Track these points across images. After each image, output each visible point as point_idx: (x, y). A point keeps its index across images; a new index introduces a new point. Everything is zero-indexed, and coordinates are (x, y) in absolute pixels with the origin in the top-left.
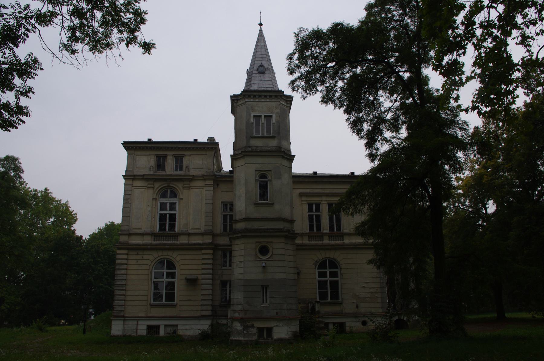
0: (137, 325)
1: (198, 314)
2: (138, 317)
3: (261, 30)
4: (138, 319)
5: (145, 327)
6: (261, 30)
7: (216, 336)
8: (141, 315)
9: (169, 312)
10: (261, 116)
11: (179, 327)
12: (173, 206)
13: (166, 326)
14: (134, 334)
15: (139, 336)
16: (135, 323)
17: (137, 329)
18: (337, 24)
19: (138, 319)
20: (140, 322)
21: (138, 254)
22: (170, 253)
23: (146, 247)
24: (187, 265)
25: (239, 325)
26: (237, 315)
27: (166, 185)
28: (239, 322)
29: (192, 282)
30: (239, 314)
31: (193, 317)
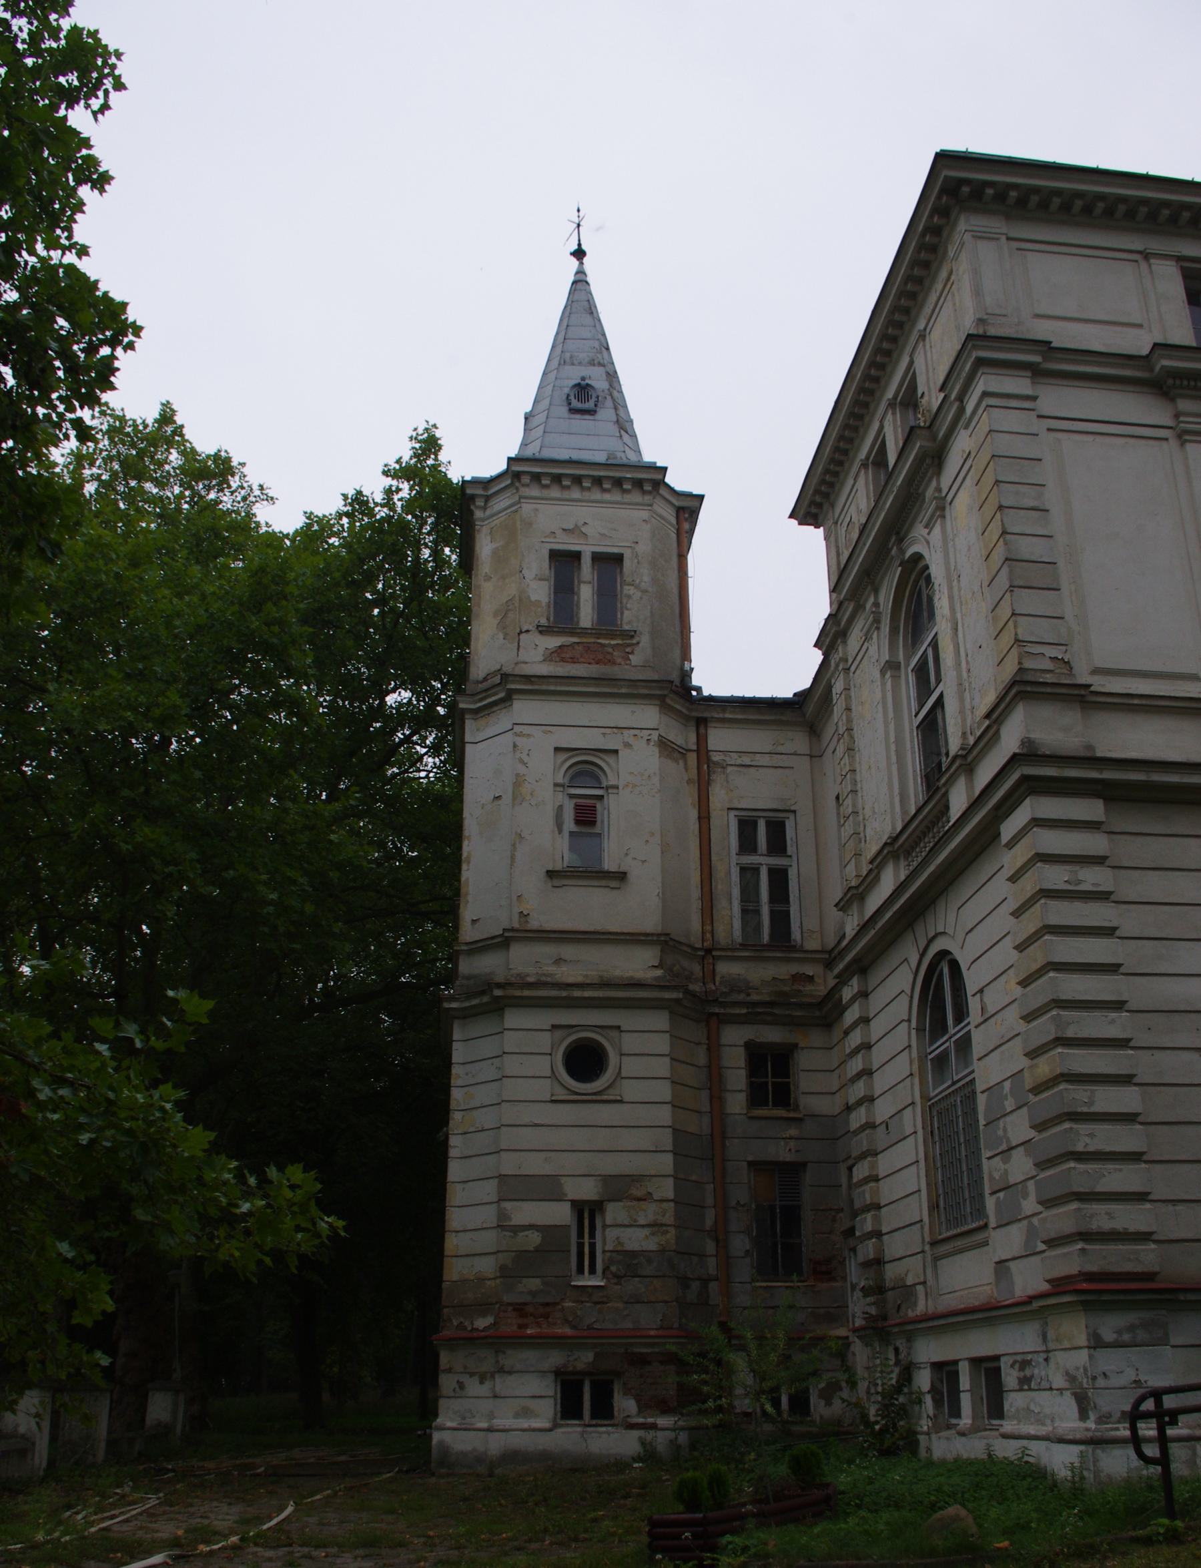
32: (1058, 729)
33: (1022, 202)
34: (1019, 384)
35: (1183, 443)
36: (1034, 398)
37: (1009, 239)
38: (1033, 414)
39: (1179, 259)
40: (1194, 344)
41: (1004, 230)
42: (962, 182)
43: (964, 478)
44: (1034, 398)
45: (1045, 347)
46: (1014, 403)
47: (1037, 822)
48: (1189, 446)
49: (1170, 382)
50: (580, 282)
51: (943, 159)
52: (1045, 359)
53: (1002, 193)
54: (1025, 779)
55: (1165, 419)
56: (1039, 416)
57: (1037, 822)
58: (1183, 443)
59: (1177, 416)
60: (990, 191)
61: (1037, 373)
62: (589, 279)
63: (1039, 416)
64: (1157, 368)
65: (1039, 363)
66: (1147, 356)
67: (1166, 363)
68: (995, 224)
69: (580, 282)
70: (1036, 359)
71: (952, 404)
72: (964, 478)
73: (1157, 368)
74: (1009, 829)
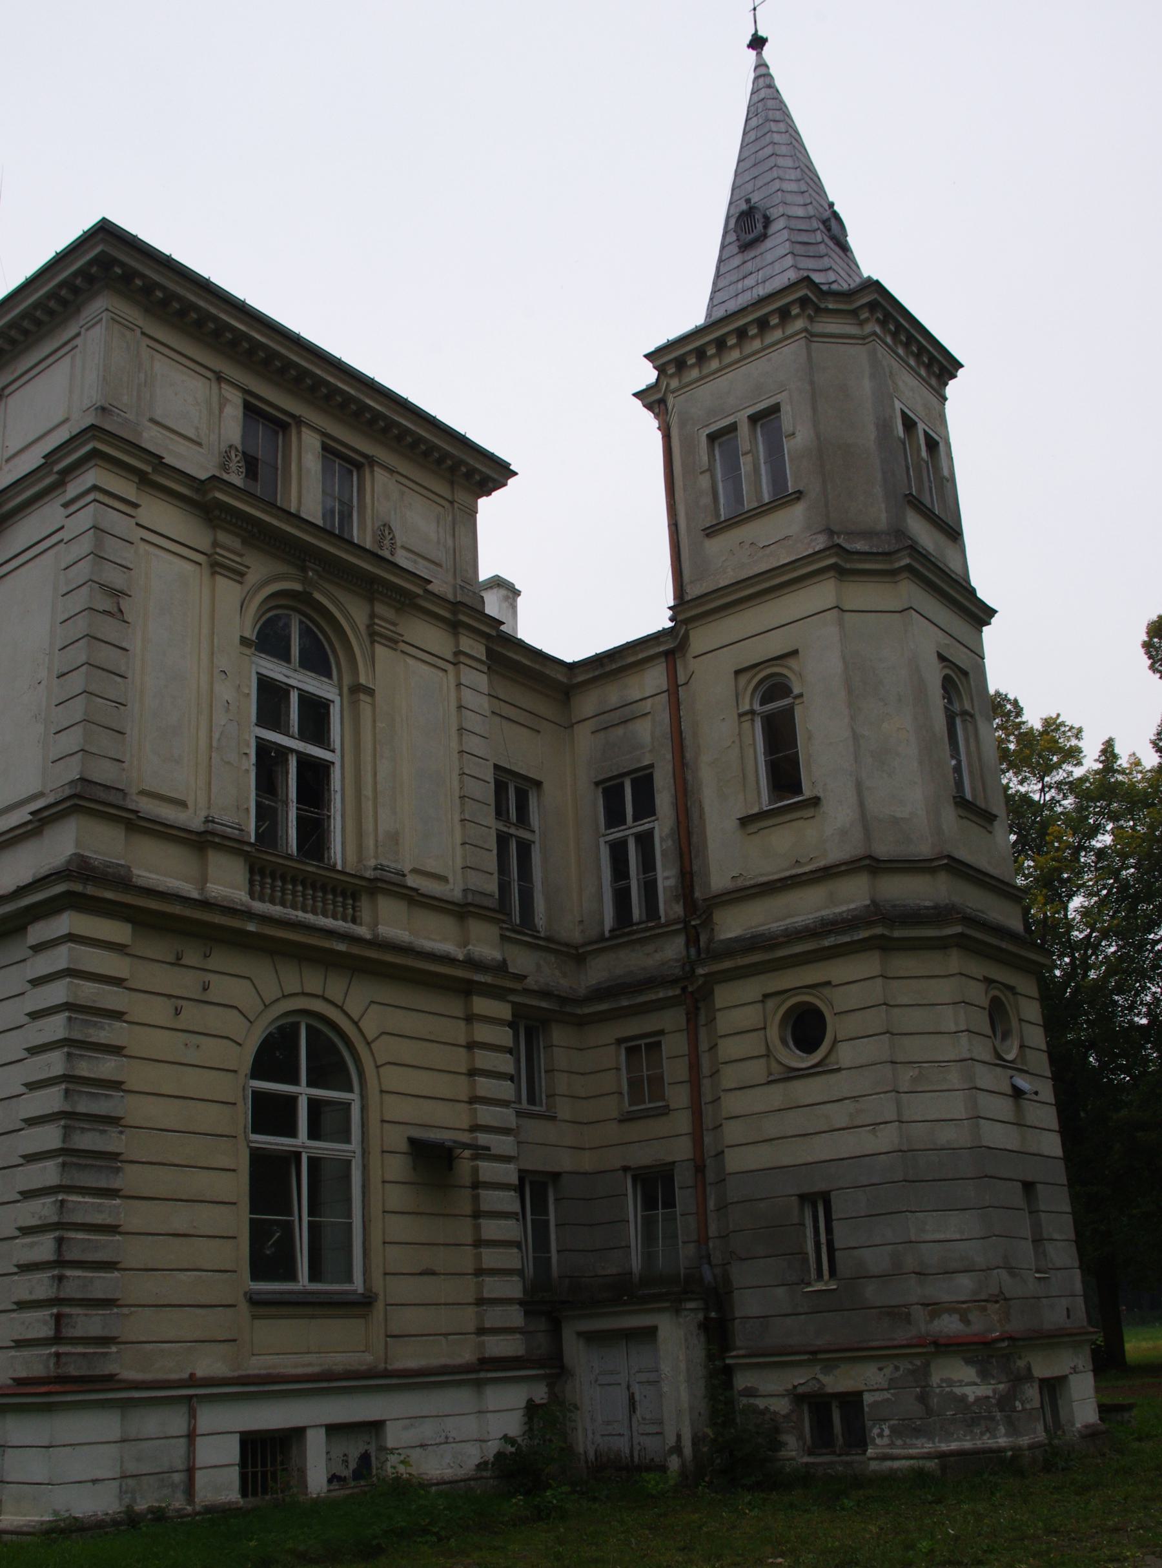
0: (191, 1436)
1: (467, 1356)
2: (193, 1381)
3: (761, 65)
4: (191, 1393)
5: (231, 1451)
6: (761, 65)
7: (735, 1458)
8: (210, 1365)
9: (335, 1344)
10: (733, 428)
11: (394, 1436)
12: (316, 716)
13: (333, 1430)
14: (178, 1502)
15: (209, 1509)
16: (177, 1423)
17: (190, 1471)
18: (105, 232)
19: (191, 1393)
20: (209, 1418)
21: (177, 963)
22: (335, 988)
23: (980, 877)
24: (416, 1071)
25: (969, 1373)
26: (949, 1325)
27: (297, 587)
28: (968, 1362)
29: (432, 1160)
30: (965, 1321)
31: (327, 1376)
32: (105, 844)
33: (164, 303)
34: (126, 488)
35: (214, 573)
36: (136, 506)
37: (143, 333)
38: (133, 521)
39: (324, 434)
40: (320, 523)
41: (140, 323)
42: (115, 261)
43: (895, 1347)
44: (136, 506)
45: (157, 460)
46: (117, 504)
47: (71, 938)
48: (218, 578)
49: (217, 513)
50: (763, 77)
51: (105, 231)
52: (154, 470)
53: (149, 288)
54: (69, 894)
55: (204, 543)
56: (137, 524)
57: (71, 938)
58: (214, 573)
59: (215, 544)
60: (138, 282)
61: (143, 480)
62: (772, 71)
63: (137, 524)
64: (210, 496)
65: (147, 473)
66: (202, 482)
67: (218, 495)
68: (133, 314)
69: (763, 77)
70: (149, 469)
71: (50, 473)
72: (895, 1347)
73: (210, 496)
74: (38, 932)
